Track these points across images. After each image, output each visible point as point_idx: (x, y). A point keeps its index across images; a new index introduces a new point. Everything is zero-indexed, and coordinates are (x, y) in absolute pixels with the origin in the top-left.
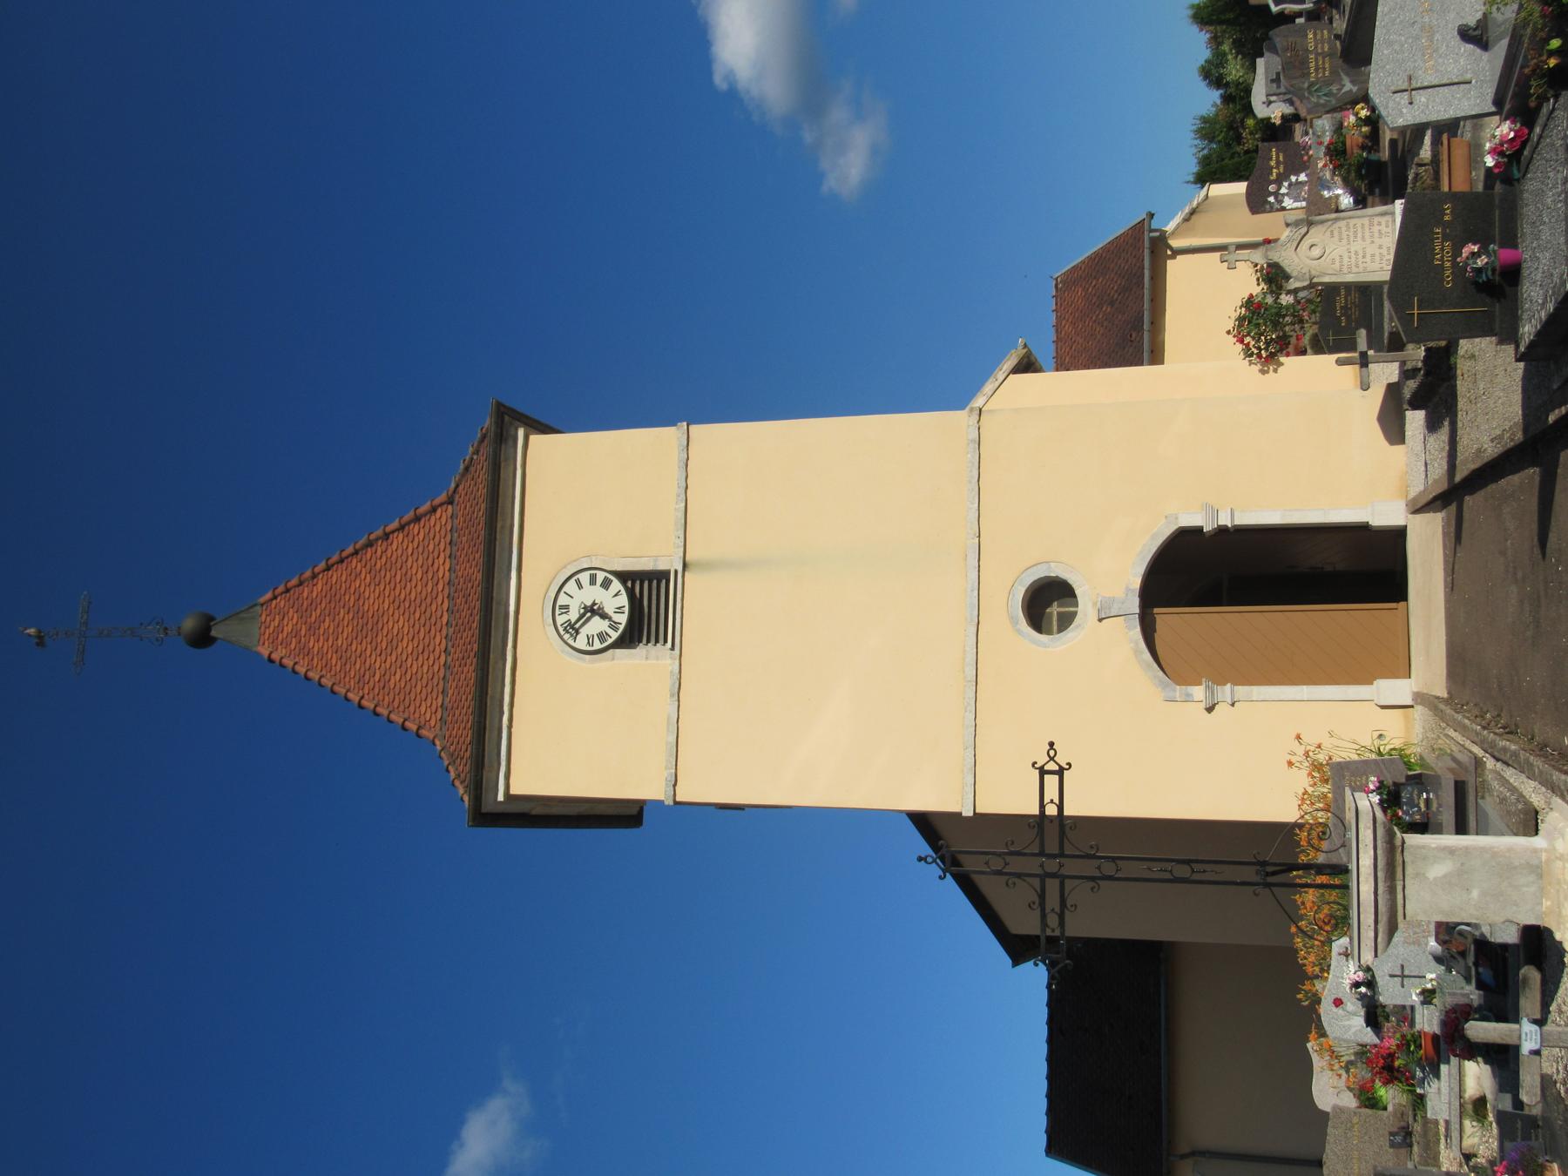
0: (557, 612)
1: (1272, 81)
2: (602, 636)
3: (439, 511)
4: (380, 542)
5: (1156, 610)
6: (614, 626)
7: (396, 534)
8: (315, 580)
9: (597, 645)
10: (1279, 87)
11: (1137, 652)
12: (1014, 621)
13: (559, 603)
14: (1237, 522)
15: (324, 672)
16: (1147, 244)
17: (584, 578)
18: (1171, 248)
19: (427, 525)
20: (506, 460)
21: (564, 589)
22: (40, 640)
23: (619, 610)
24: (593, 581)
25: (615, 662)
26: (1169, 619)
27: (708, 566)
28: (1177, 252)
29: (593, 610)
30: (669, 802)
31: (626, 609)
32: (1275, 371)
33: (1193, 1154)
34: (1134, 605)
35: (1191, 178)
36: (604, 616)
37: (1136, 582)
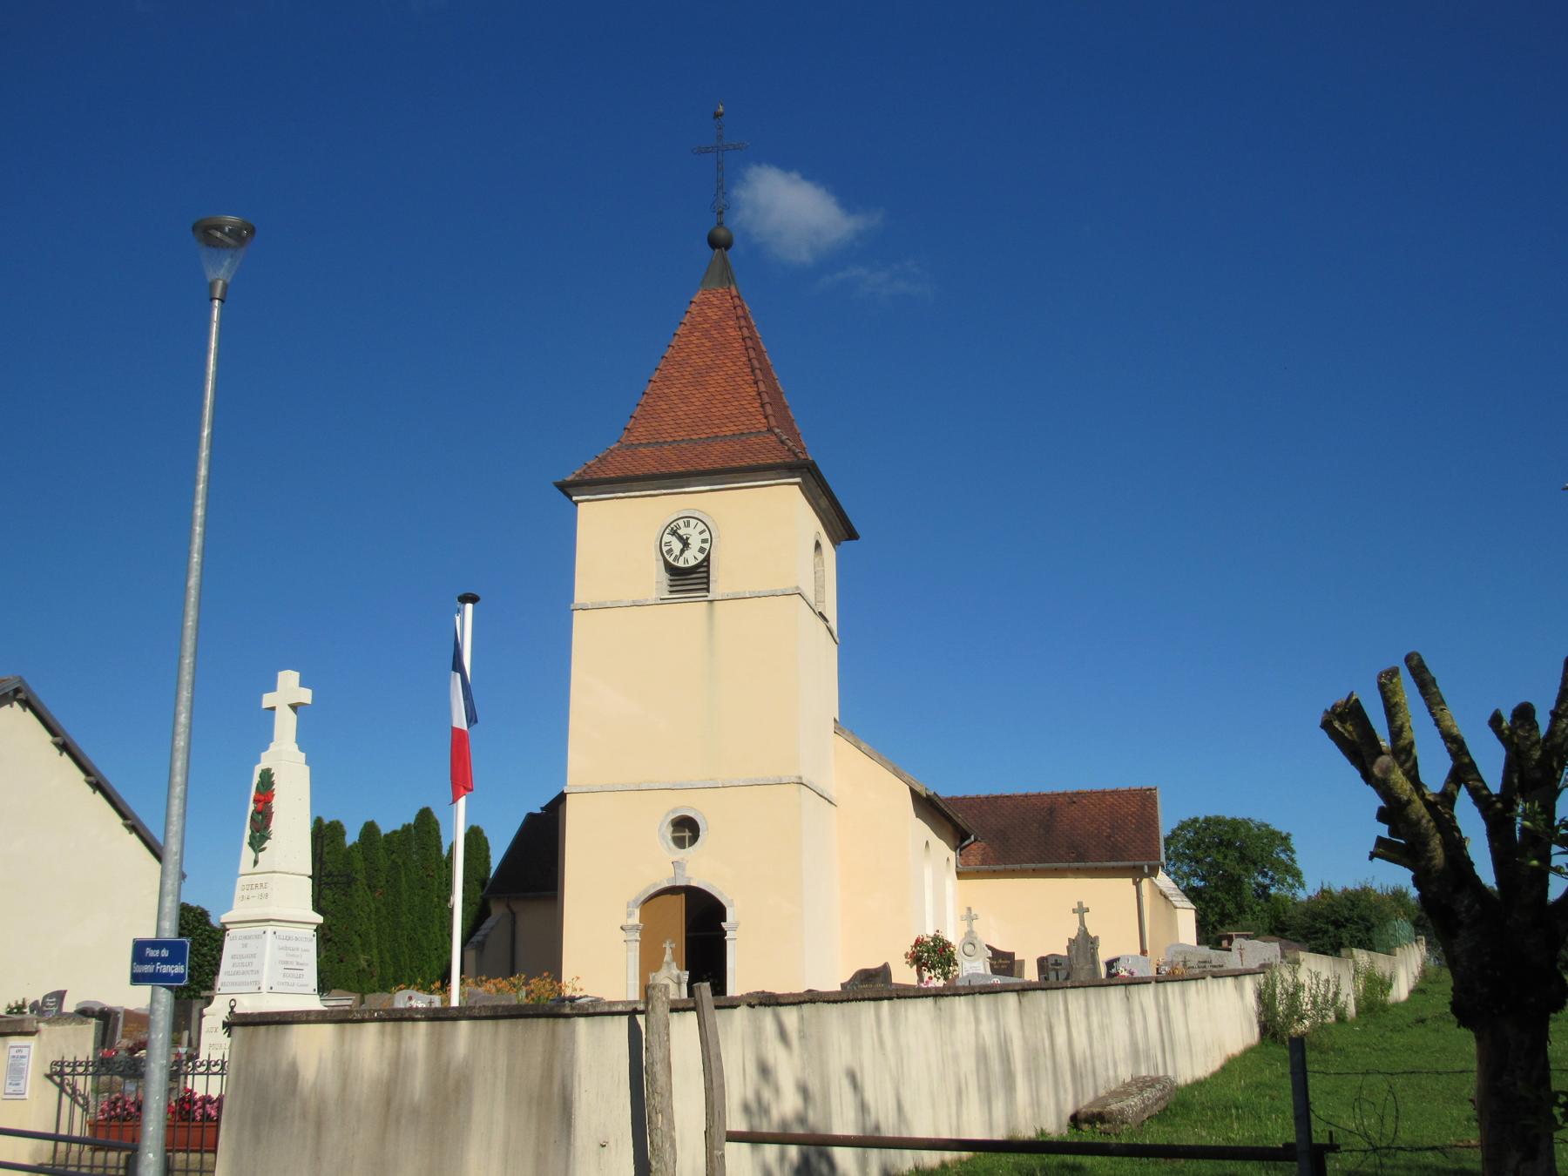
0: (685, 520)
1: (1056, 960)
2: (670, 551)
3: (765, 421)
4: (753, 377)
5: (683, 895)
6: (676, 559)
7: (756, 389)
8: (738, 329)
9: (665, 549)
10: (1052, 965)
11: (655, 885)
12: (673, 811)
13: (691, 520)
14: (728, 942)
15: (676, 348)
16: (1137, 863)
17: (706, 535)
18: (1140, 881)
19: (757, 413)
20: (778, 473)
21: (700, 522)
22: (717, 115)
23: (686, 561)
24: (704, 541)
25: (655, 562)
26: (679, 903)
27: (711, 616)
28: (1137, 884)
29: (686, 544)
30: (572, 607)
31: (687, 565)
32: (907, 963)
33: (513, 914)
34: (681, 882)
35: (1325, 887)
36: (682, 551)
37: (693, 884)
